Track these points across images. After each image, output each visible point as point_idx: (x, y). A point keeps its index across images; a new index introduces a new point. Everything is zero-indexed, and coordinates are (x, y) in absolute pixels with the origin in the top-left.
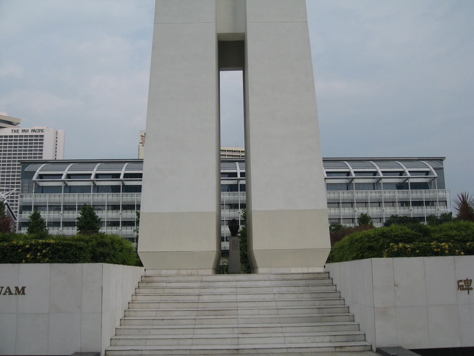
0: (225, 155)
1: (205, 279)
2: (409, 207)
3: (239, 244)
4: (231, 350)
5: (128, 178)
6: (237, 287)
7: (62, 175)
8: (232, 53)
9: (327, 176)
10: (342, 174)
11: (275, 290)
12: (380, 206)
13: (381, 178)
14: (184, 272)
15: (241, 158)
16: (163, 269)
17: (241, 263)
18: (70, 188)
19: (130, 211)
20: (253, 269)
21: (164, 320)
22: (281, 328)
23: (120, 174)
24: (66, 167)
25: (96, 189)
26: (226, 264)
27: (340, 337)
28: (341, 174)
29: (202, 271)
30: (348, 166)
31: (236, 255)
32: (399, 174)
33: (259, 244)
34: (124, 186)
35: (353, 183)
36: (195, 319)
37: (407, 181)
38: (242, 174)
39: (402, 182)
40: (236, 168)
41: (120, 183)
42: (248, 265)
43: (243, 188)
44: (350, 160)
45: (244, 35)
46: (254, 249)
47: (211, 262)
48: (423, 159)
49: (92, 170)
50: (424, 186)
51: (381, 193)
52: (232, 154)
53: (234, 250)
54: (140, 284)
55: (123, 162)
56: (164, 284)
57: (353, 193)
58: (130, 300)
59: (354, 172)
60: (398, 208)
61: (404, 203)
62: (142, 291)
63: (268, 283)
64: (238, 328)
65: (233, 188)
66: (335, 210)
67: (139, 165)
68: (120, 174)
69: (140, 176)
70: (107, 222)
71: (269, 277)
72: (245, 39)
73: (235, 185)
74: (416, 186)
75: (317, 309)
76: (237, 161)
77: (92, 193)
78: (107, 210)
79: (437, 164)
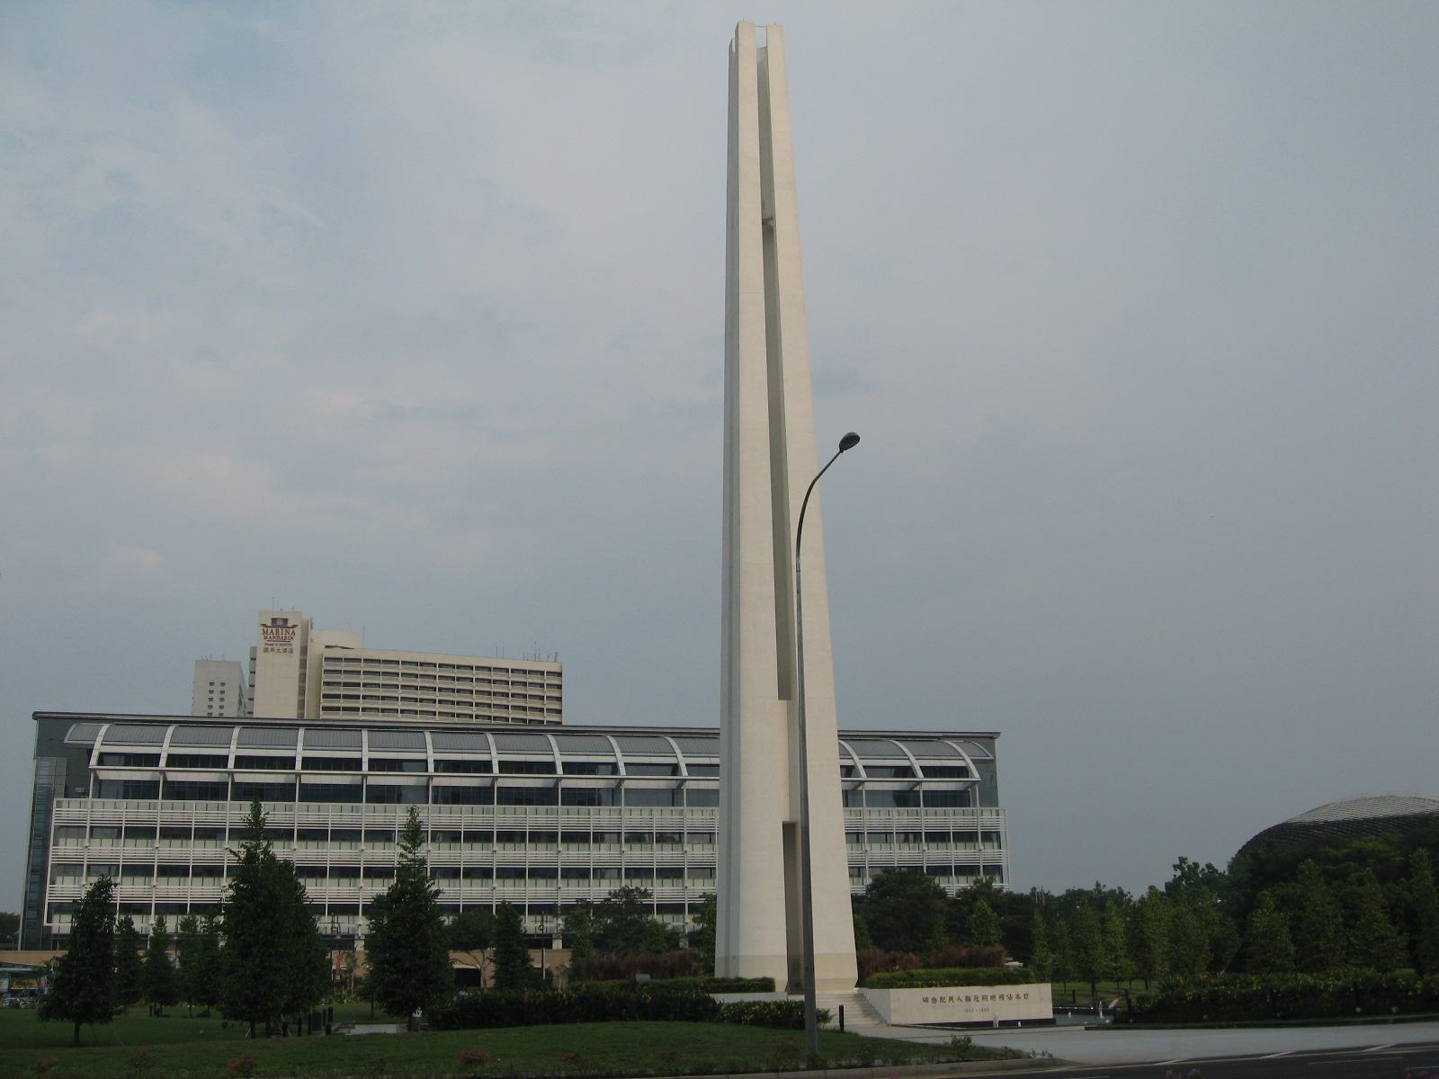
10: (651, 768)
19: (314, 844)
23: (158, 756)
37: (917, 788)
39: (907, 789)
49: (227, 746)
50: (957, 799)
55: (164, 722)
60: (896, 846)
61: (910, 837)
66: (113, 846)
68: (158, 756)
73: (548, 789)
74: (935, 799)
76: (427, 728)
79: (980, 751)
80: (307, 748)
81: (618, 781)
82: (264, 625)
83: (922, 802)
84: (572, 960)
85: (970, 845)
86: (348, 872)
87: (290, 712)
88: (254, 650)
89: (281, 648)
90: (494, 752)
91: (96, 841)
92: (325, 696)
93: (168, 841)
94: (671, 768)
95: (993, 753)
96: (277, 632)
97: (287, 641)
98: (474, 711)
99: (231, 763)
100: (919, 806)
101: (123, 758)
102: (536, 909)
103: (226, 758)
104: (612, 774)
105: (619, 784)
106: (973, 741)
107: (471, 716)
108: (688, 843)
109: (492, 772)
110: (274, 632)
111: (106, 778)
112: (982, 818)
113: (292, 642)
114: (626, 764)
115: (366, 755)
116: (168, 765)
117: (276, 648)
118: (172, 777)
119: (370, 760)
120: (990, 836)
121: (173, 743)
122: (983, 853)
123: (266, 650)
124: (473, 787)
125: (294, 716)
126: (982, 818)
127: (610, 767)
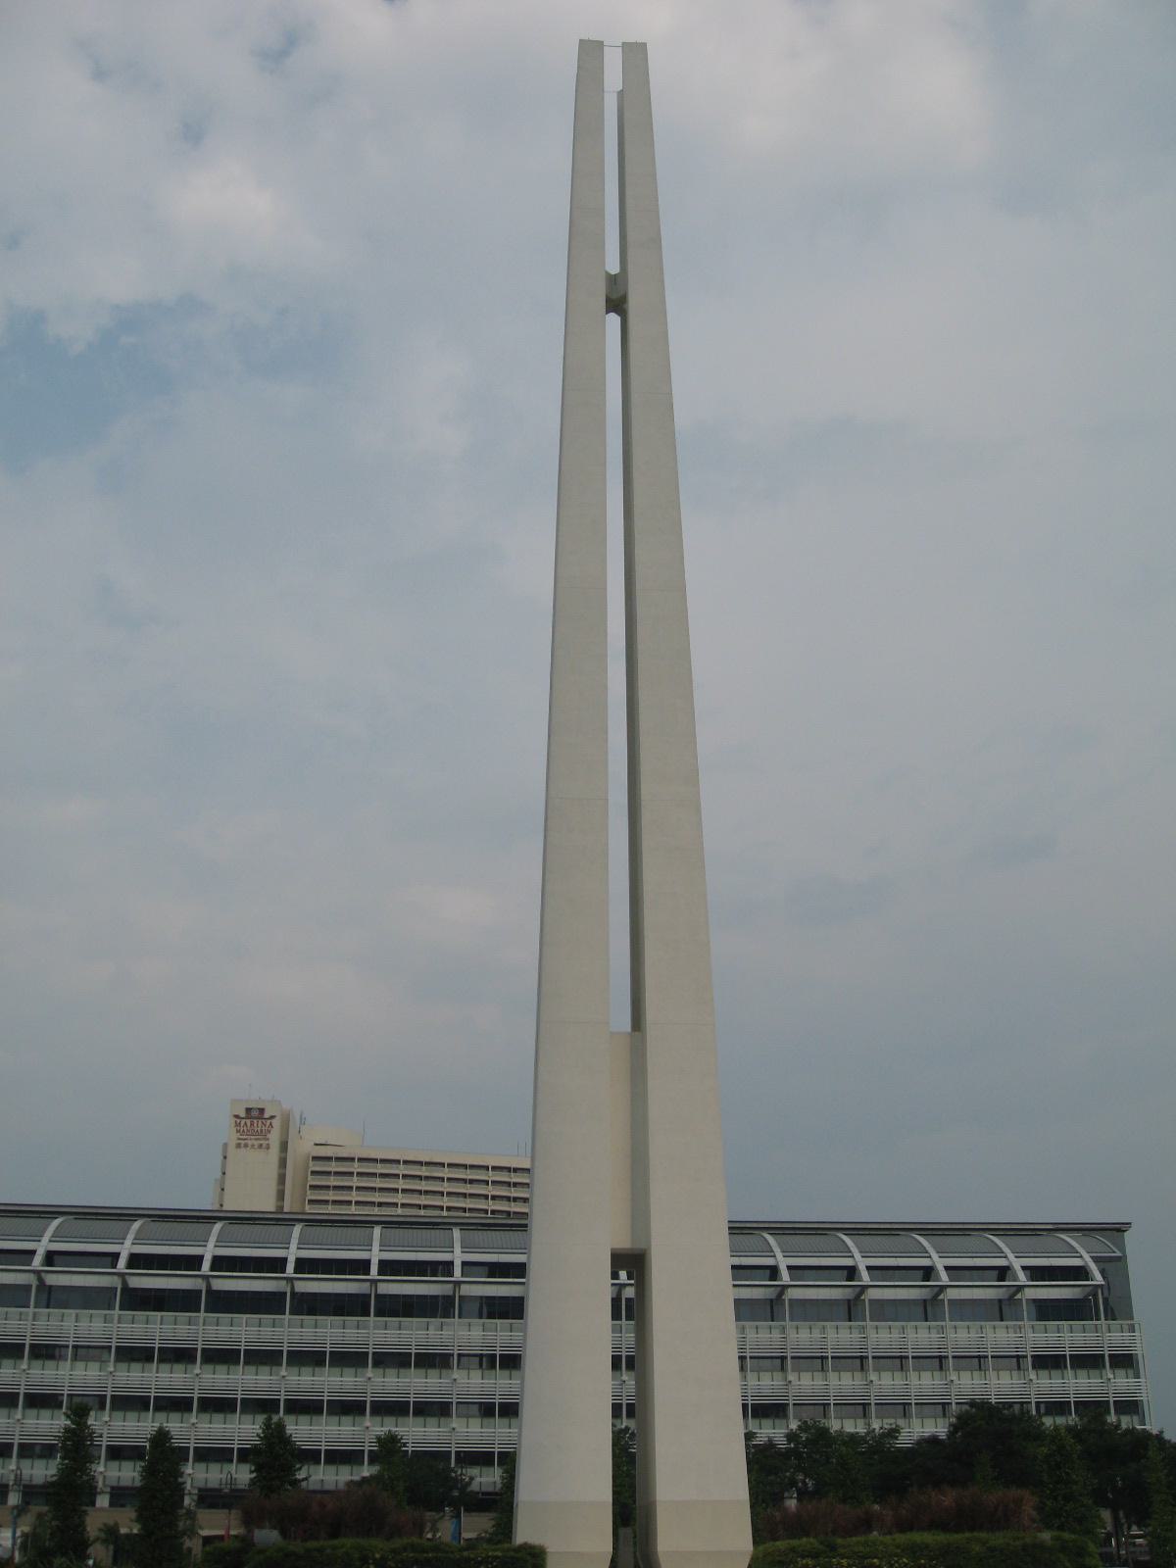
2: (1104, 1372)
5: (509, 1277)
7: (33, 1252)
9: (792, 1280)
10: (807, 1272)
12: (941, 1368)
13: (943, 1288)
15: (489, 1215)
23: (200, 1258)
25: (45, 1296)
28: (786, 1273)
30: (852, 1249)
32: (995, 1273)
34: (126, 1289)
35: (864, 1300)
40: (772, 1254)
41: (200, 1284)
44: (857, 1230)
49: (121, 1241)
51: (1023, 1330)
55: (125, 1216)
57: (783, 1329)
59: (867, 1267)
67: (513, 1237)
68: (200, 1258)
69: (518, 1270)
70: (68, 1395)
73: (444, 1297)
78: (72, 1360)
80: (735, 1254)
81: (779, 1289)
82: (237, 1116)
83: (947, 1315)
84: (140, 1519)
85: (1094, 1372)
86: (349, 1408)
87: (266, 1203)
88: (225, 1145)
89: (256, 1143)
90: (458, 1249)
91: (80, 1365)
92: (313, 1187)
93: (424, 1371)
94: (768, 1272)
95: (1122, 1249)
96: (252, 1124)
97: (263, 1134)
98: (446, 1202)
99: (290, 1267)
100: (1023, 1320)
101: (486, 1268)
102: (206, 1455)
103: (284, 1260)
104: (847, 1280)
105: (781, 1294)
106: (1093, 1234)
107: (441, 1208)
108: (793, 1370)
109: (452, 1276)
110: (249, 1124)
111: (468, 1294)
112: (1104, 1336)
113: (269, 1136)
114: (789, 1268)
115: (375, 1256)
116: (212, 1269)
117: (250, 1143)
118: (219, 1285)
119: (381, 1262)
120: (1125, 1361)
121: (219, 1244)
122: (1115, 1384)
123: (238, 1146)
124: (431, 1296)
125: (272, 1209)
126: (1104, 1336)
127: (768, 1272)
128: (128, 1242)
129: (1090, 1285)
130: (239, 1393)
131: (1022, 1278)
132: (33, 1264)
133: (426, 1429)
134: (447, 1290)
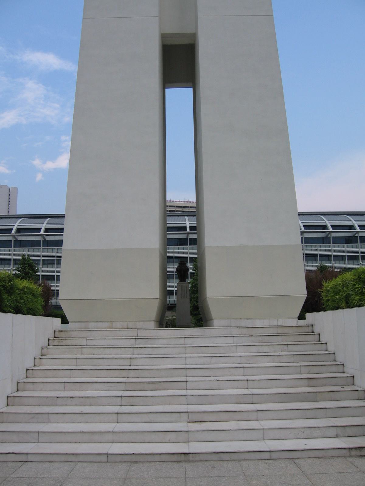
0: (175, 211)
1: (142, 334)
3: (188, 294)
4: (176, 456)
6: (186, 346)
8: (179, 62)
11: (240, 351)
14: (119, 325)
16: (91, 322)
17: (191, 314)
18: (20, 243)
20: (206, 321)
21: (73, 397)
22: (255, 413)
24: (16, 222)
26: (175, 318)
27: (353, 428)
29: (141, 323)
31: (185, 306)
33: (214, 289)
34: (45, 241)
36: (122, 397)
37: (356, 235)
38: (192, 228)
42: (199, 317)
43: (194, 242)
45: (194, 36)
46: (208, 295)
47: (153, 311)
48: (61, 216)
52: (182, 210)
53: (183, 298)
54: (50, 341)
56: (84, 342)
58: (29, 364)
62: (51, 351)
63: (229, 341)
64: (188, 412)
65: (182, 242)
71: (231, 332)
72: (195, 41)
75: (306, 381)
76: (186, 216)
77: (42, 248)
78: (57, 264)
128: (16, 225)
129: (355, 231)
130: (56, 273)
131: (331, 229)
132: (41, 232)
133: (170, 283)
134: (184, 236)
